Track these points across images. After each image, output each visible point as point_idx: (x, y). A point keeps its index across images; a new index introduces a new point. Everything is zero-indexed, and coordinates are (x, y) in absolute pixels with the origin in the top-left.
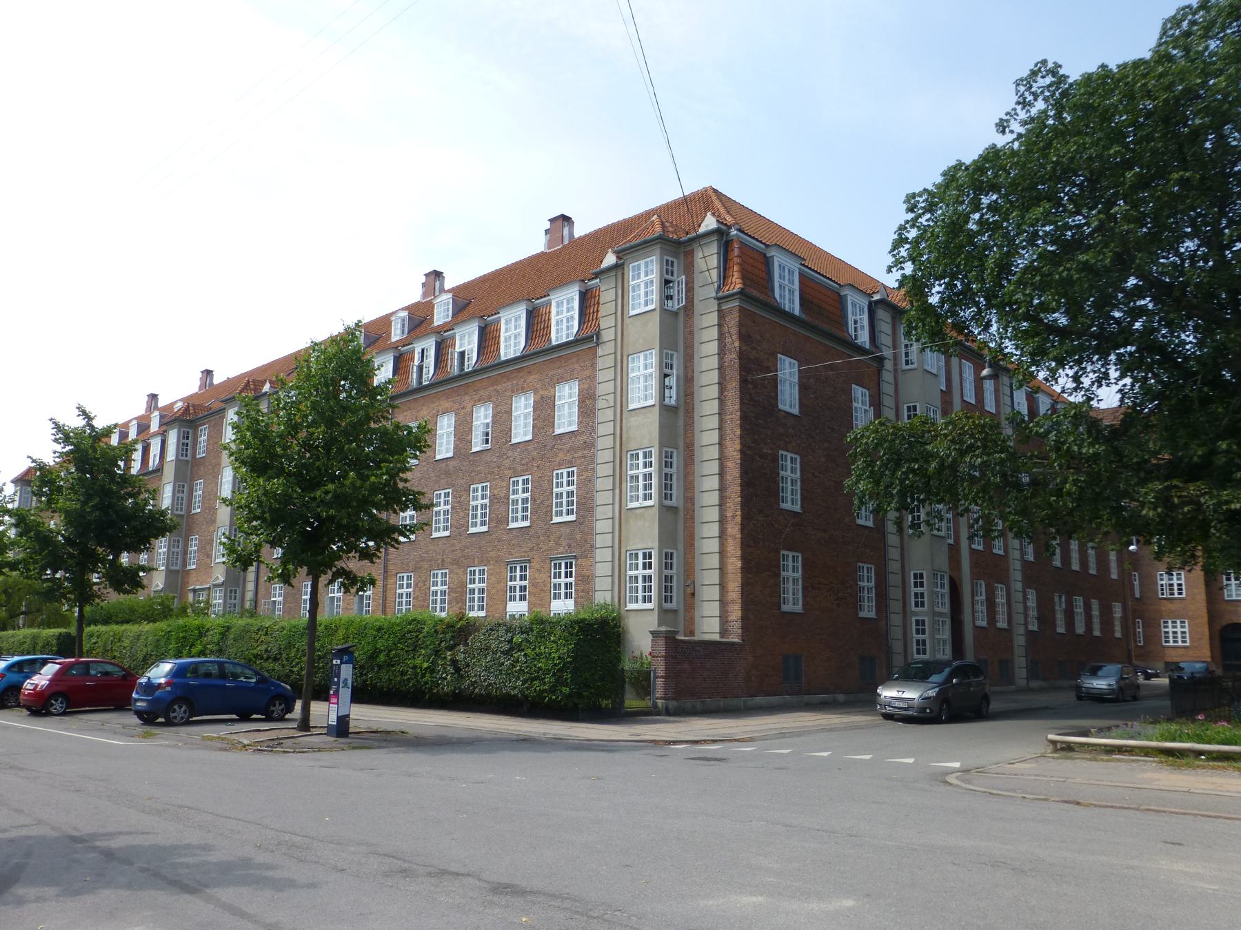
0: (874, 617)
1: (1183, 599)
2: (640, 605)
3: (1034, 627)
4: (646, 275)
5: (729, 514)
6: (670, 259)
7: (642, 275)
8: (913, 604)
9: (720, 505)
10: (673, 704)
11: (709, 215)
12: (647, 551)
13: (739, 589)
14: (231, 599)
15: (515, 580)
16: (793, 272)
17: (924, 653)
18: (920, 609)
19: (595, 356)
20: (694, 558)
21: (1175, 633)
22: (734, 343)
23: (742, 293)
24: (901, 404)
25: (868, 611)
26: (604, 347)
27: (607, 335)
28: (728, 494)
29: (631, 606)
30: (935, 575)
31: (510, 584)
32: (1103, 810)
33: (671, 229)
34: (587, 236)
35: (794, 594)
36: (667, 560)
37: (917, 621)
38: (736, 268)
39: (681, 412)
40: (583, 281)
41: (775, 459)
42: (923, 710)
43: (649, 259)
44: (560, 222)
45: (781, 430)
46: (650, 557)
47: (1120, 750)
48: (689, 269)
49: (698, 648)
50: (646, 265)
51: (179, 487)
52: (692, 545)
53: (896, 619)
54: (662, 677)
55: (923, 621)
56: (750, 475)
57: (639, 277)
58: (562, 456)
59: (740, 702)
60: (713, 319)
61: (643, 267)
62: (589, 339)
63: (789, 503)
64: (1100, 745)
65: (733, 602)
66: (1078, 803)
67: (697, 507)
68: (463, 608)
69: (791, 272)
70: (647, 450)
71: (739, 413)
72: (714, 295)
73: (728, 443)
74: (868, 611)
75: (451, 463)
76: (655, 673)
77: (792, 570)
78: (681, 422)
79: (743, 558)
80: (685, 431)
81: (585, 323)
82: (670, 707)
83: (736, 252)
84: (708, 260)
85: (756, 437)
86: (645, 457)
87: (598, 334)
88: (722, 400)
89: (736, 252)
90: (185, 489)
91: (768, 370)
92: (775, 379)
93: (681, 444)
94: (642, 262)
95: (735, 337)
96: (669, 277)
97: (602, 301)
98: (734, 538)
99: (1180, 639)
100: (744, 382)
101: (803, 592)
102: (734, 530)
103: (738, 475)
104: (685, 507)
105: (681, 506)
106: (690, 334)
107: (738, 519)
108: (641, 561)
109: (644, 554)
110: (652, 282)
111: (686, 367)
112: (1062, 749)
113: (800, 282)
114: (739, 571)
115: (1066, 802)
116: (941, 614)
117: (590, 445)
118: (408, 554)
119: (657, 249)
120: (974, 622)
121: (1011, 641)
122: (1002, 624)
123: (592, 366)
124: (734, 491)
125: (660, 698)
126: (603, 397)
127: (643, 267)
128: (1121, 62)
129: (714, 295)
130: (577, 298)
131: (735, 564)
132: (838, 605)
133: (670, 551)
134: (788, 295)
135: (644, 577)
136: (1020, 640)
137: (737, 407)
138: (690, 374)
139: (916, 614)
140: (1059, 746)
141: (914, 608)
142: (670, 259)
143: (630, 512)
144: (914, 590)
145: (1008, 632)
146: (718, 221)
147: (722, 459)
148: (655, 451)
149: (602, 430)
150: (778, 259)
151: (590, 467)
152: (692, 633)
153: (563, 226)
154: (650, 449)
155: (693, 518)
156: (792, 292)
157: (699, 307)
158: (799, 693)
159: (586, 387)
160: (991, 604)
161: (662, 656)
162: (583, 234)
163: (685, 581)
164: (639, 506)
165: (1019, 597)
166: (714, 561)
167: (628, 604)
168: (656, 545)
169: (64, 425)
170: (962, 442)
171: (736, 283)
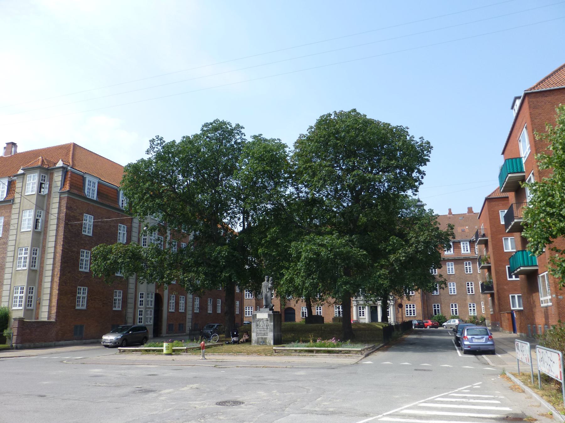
2: (17, 308)
3: (197, 311)
4: (33, 180)
5: (56, 273)
7: (32, 180)
9: (52, 270)
10: (19, 345)
11: (60, 160)
12: (22, 287)
13: (56, 301)
14: (32, 267)
15: (17, 294)
16: (95, 183)
18: (141, 306)
19: (11, 208)
20: (41, 289)
21: (249, 311)
22: (64, 210)
23: (68, 191)
25: (118, 307)
26: (15, 205)
27: (17, 201)
28: (56, 266)
29: (14, 308)
30: (148, 294)
33: (46, 163)
34: (22, 153)
35: (82, 302)
36: (30, 290)
37: (140, 311)
38: (68, 182)
39: (42, 233)
40: (9, 177)
42: (116, 343)
43: (35, 174)
44: (11, 145)
45: (82, 242)
46: (23, 289)
47: (149, 350)
48: (51, 180)
49: (34, 324)
50: (34, 176)
52: (41, 285)
53: (130, 311)
54: (16, 335)
55: (142, 311)
56: (66, 259)
57: (30, 181)
59: (53, 343)
60: (57, 200)
61: (32, 177)
62: (9, 201)
63: (84, 269)
64: (131, 350)
65: (54, 306)
66: (84, 364)
67: (44, 270)
69: (94, 183)
70: (26, 248)
71: (63, 236)
72: (58, 191)
73: (58, 247)
74: (118, 307)
76: (13, 333)
77: (83, 294)
78: (42, 238)
79: (59, 290)
80: (43, 241)
81: (9, 194)
82: (18, 346)
83: (69, 176)
84: (58, 177)
85: (70, 245)
86: (25, 250)
87: (13, 200)
88: (57, 230)
89: (69, 176)
90: (38, 252)
91: (79, 220)
92: (81, 225)
93: (41, 246)
94: (32, 175)
95: (65, 208)
96: (43, 182)
97: (16, 187)
98: (56, 282)
100: (66, 224)
101: (87, 302)
102: (57, 279)
103: (60, 259)
104: (40, 270)
105: (38, 270)
106: (49, 205)
107: (59, 275)
108: (19, 291)
109: (21, 288)
110: (35, 183)
111: (46, 217)
114: (57, 295)
115: (174, 370)
116: (149, 308)
117: (6, 243)
119: (38, 171)
120: (168, 310)
121: (186, 317)
122: (182, 310)
123: (10, 212)
124: (58, 264)
125: (14, 343)
126: (13, 225)
127: (32, 177)
128: (194, 134)
129: (58, 191)
130: (7, 184)
131: (56, 292)
133: (32, 287)
134: (91, 191)
135: (20, 297)
136: (189, 316)
137: (63, 234)
138: (47, 220)
139: (140, 308)
140: (121, 351)
141: (139, 306)
142: (44, 175)
143: (17, 272)
144: (140, 299)
145: (185, 314)
146: (63, 163)
147: (55, 253)
148: (29, 249)
149: (11, 238)
150: (88, 178)
151: (5, 252)
152: (38, 318)
153: (12, 147)
155: (42, 274)
156: (93, 191)
157: (53, 195)
158: (81, 339)
159: (7, 220)
160: (177, 304)
161: (16, 328)
163: (37, 299)
164: (21, 269)
165: (191, 300)
166: (48, 291)
167: (13, 307)
168: (26, 284)
170: (118, 255)
171: (67, 188)
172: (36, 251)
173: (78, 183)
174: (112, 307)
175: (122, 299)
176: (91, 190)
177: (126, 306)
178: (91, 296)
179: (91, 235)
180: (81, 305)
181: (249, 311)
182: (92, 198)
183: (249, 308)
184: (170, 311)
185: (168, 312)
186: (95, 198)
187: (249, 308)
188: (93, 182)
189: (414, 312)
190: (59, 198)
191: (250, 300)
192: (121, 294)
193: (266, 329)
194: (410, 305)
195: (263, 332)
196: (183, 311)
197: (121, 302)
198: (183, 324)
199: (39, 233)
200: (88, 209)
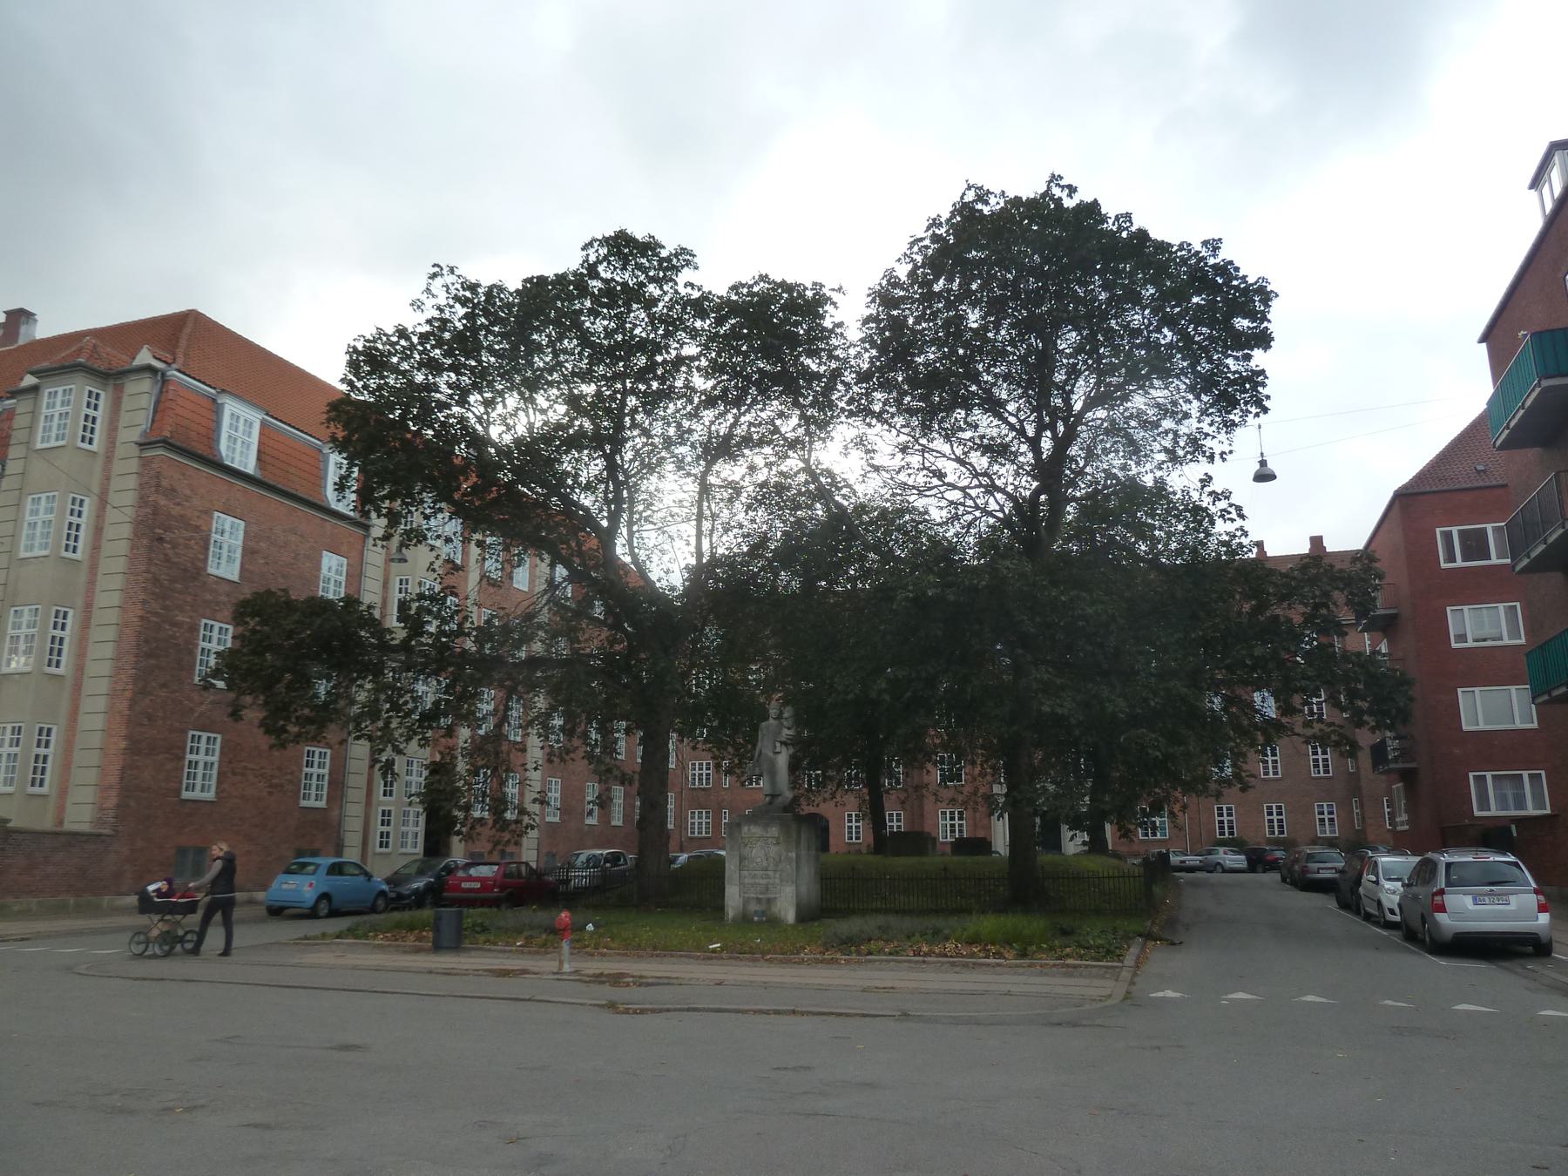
0: (325, 807)
1: (1330, 778)
6: (95, 390)
8: (382, 792)
12: (46, 726)
16: (251, 424)
17: (387, 847)
18: (388, 798)
32: (825, 1017)
41: (194, 629)
93: (80, 602)
94: (60, 390)
101: (218, 778)
113: (261, 434)
132: (270, 793)
139: (380, 803)
142: (95, 390)
154: (66, 609)
162: (50, 334)
169: (880, 284)
172: (65, 617)
178: (230, 762)
181: (700, 823)
183: (700, 813)
186: (250, 466)
192: (328, 761)
195: (761, 881)
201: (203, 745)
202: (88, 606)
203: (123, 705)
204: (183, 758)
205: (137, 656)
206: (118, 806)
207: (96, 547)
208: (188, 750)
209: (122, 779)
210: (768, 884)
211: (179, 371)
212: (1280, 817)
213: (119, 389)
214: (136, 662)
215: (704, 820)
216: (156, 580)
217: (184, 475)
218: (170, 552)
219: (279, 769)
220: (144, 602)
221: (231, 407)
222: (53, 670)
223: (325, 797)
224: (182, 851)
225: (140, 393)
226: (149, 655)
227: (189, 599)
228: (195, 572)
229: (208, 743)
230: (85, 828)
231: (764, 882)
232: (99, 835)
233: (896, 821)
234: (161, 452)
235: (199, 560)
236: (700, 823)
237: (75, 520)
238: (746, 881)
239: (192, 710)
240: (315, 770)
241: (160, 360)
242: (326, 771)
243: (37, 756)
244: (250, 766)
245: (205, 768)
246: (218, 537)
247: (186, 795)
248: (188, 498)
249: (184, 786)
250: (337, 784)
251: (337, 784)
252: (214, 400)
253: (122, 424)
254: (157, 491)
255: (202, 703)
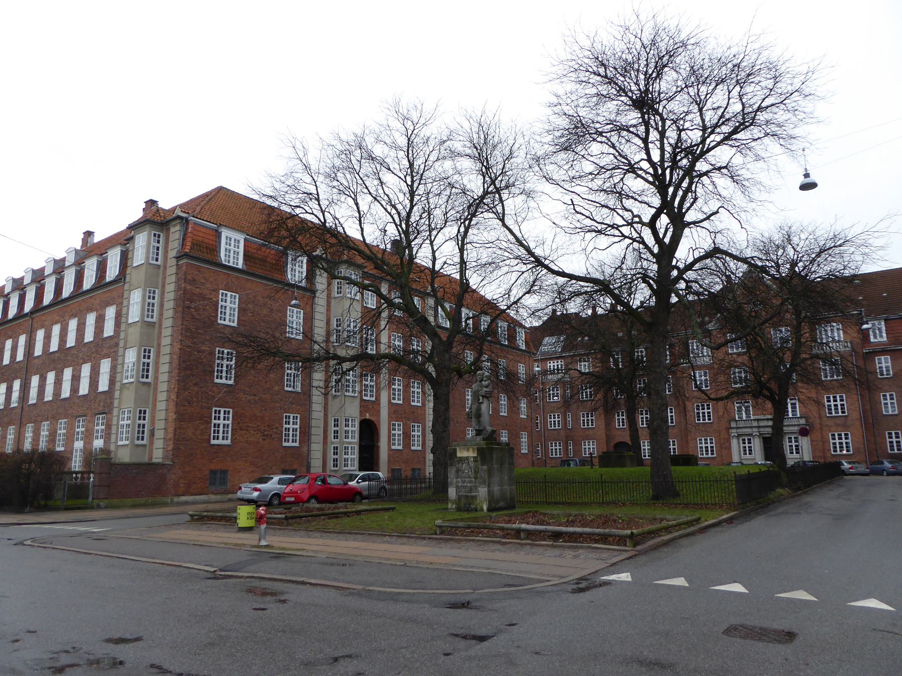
6: (157, 233)
12: (143, 409)
16: (239, 241)
18: (336, 440)
24: (332, 318)
31: (285, 426)
41: (212, 354)
51: (145, 352)
58: (105, 351)
68: (54, 446)
75: (57, 355)
90: (152, 354)
93: (155, 344)
99: (895, 448)
105: (152, 383)
112: (197, 520)
118: (32, 412)
119: (148, 227)
139: (332, 443)
142: (157, 233)
172: (149, 352)
173: (206, 241)
174: (280, 440)
175: (300, 428)
176: (232, 252)
177: (309, 440)
178: (239, 423)
179: (235, 324)
180: (221, 437)
181: (556, 449)
182: (227, 264)
183: (556, 443)
184: (393, 447)
185: (390, 449)
186: (240, 265)
187: (556, 443)
188: (235, 240)
189: (709, 416)
190: (175, 267)
191: (556, 432)
192: (298, 421)
193: (473, 480)
194: (840, 435)
195: (469, 485)
196: (420, 448)
197: (298, 433)
198: (419, 469)
199: (151, 325)
200: (228, 283)
201: (222, 415)
202: (159, 345)
203: (173, 397)
204: (211, 422)
205: (179, 369)
206: (173, 449)
207: (161, 314)
208: (213, 418)
209: (175, 434)
210: (471, 487)
211: (194, 216)
212: (891, 440)
213: (168, 230)
214: (179, 373)
215: (591, 447)
216: (187, 329)
217: (200, 272)
218: (195, 314)
219: (269, 426)
220: (181, 341)
221: (225, 233)
222: (145, 380)
223: (298, 441)
224: (214, 472)
225: (176, 231)
226: (186, 369)
227: (208, 338)
228: (211, 322)
229: (225, 414)
230: (160, 460)
231: (469, 485)
232: (164, 465)
233: (674, 447)
234: (185, 261)
235: (212, 316)
236: (556, 449)
237: (151, 301)
238: (460, 484)
239: (214, 397)
240: (291, 426)
241: (185, 212)
242: (298, 426)
243: (139, 425)
244: (251, 425)
245: (293, 431)
246: (223, 303)
247: (213, 442)
248: (203, 284)
249: (212, 437)
250: (305, 433)
251: (305, 433)
252: (217, 231)
253: (170, 248)
254: (185, 282)
255: (219, 393)
